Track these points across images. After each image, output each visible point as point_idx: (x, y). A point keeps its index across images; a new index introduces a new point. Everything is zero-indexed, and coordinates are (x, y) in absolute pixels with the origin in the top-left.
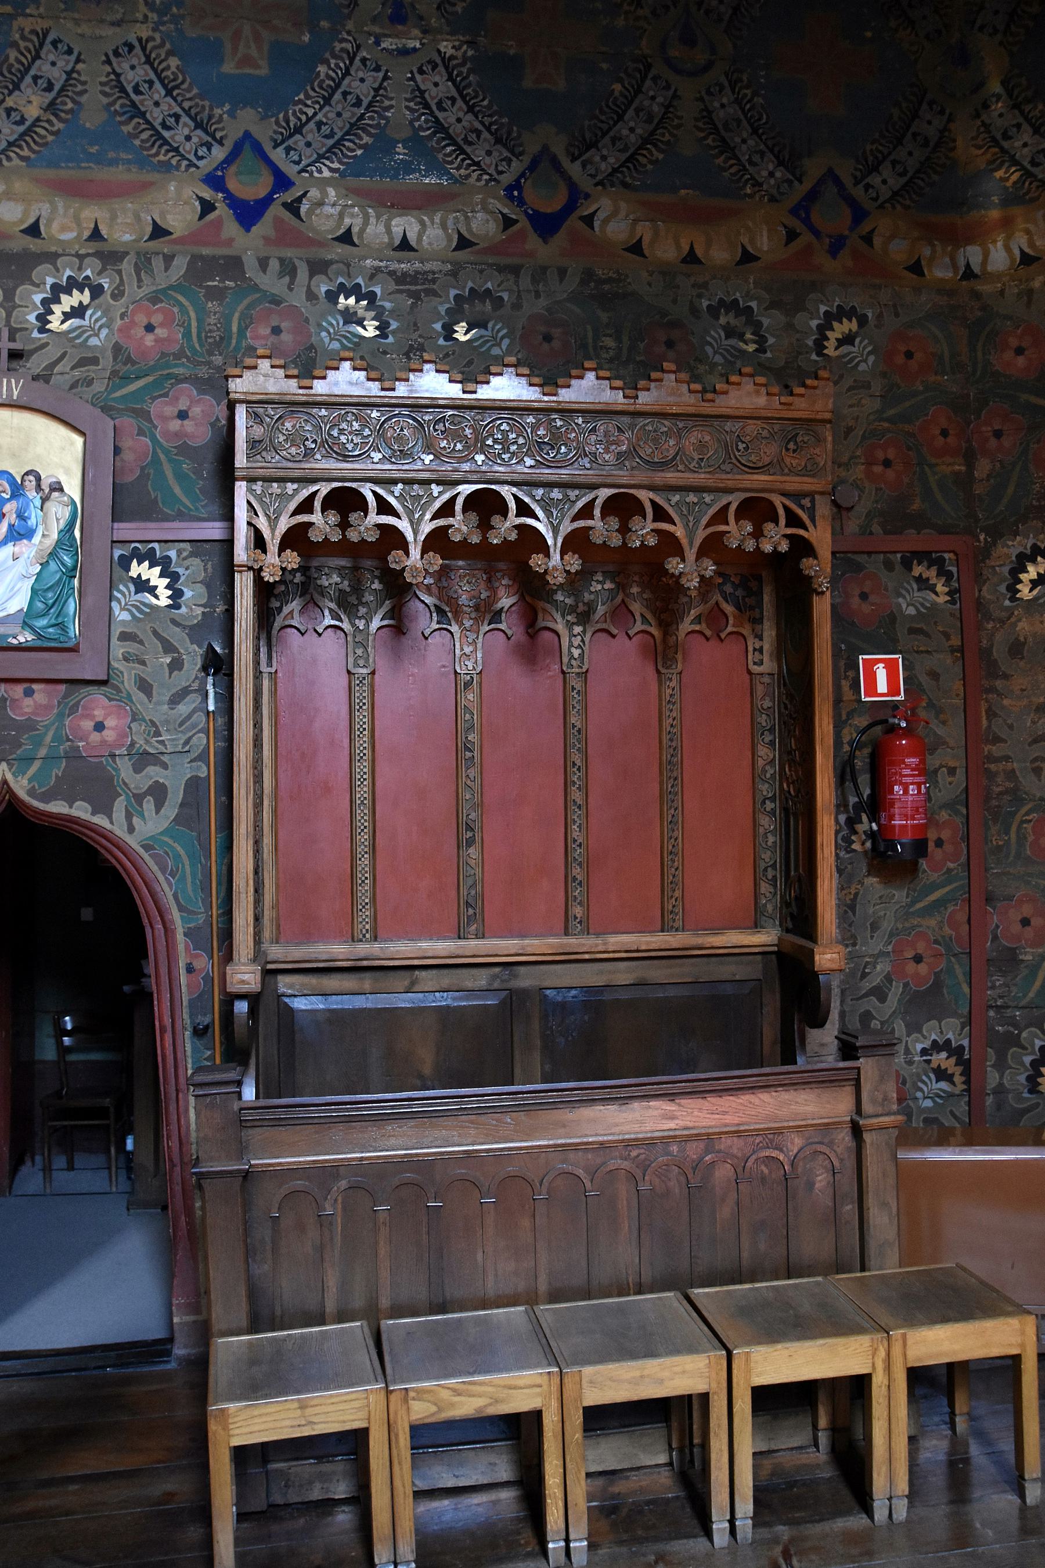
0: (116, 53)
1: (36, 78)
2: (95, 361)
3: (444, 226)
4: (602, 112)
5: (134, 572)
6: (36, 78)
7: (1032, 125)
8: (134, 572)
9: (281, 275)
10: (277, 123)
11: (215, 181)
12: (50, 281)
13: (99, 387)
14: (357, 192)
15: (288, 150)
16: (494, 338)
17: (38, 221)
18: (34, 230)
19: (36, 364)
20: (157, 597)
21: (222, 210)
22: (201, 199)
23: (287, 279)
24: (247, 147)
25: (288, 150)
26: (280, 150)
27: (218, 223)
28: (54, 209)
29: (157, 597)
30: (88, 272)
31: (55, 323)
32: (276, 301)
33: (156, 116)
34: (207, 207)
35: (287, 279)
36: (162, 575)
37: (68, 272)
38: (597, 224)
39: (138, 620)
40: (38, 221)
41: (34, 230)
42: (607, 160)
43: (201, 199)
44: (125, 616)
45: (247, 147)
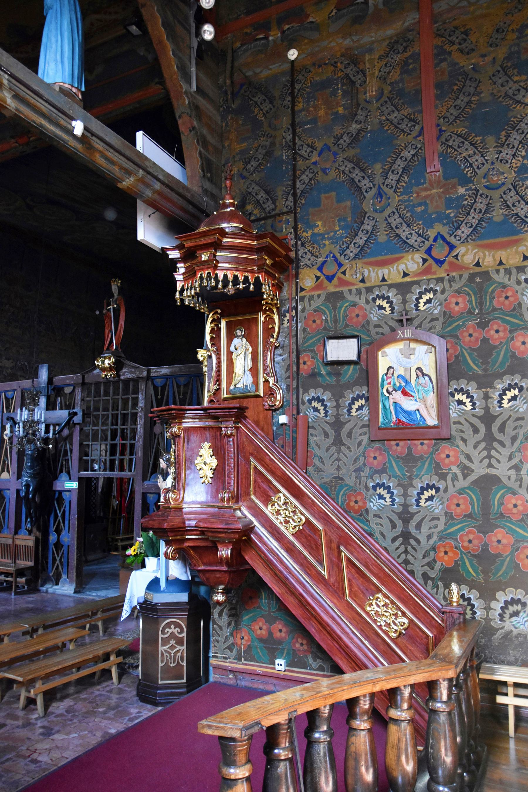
0: (505, 193)
1: (363, 231)
2: (437, 319)
3: (493, 257)
4: (460, 214)
5: (313, 405)
6: (363, 231)
7: (406, 223)
8: (313, 405)
9: (356, 295)
10: (450, 227)
11: (320, 269)
12: (418, 291)
13: (439, 328)
14: (479, 246)
15: (455, 236)
16: (434, 306)
17: (478, 261)
18: (478, 264)
19: (416, 322)
20: (466, 406)
21: (323, 277)
22: (423, 258)
23: (358, 296)
24: (439, 238)
25: (455, 236)
26: (453, 237)
27: (430, 267)
28: (485, 255)
29: (466, 406)
30: (432, 286)
31: (421, 307)
32: (504, 286)
33: (404, 235)
34: (318, 278)
35: (508, 276)
36: (467, 397)
37: (424, 287)
38: (459, 258)
39: (460, 416)
40: (478, 261)
41: (478, 264)
42: (352, 251)
43: (423, 258)
44: (455, 415)
45: (439, 238)
